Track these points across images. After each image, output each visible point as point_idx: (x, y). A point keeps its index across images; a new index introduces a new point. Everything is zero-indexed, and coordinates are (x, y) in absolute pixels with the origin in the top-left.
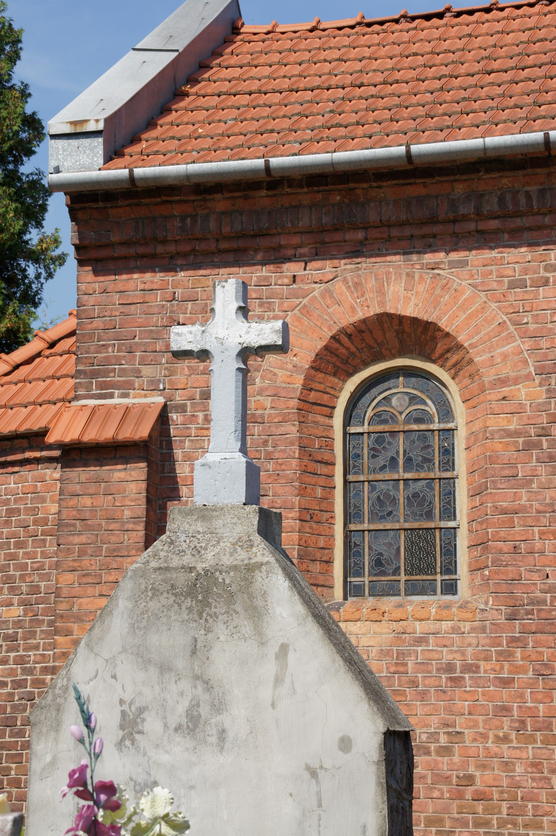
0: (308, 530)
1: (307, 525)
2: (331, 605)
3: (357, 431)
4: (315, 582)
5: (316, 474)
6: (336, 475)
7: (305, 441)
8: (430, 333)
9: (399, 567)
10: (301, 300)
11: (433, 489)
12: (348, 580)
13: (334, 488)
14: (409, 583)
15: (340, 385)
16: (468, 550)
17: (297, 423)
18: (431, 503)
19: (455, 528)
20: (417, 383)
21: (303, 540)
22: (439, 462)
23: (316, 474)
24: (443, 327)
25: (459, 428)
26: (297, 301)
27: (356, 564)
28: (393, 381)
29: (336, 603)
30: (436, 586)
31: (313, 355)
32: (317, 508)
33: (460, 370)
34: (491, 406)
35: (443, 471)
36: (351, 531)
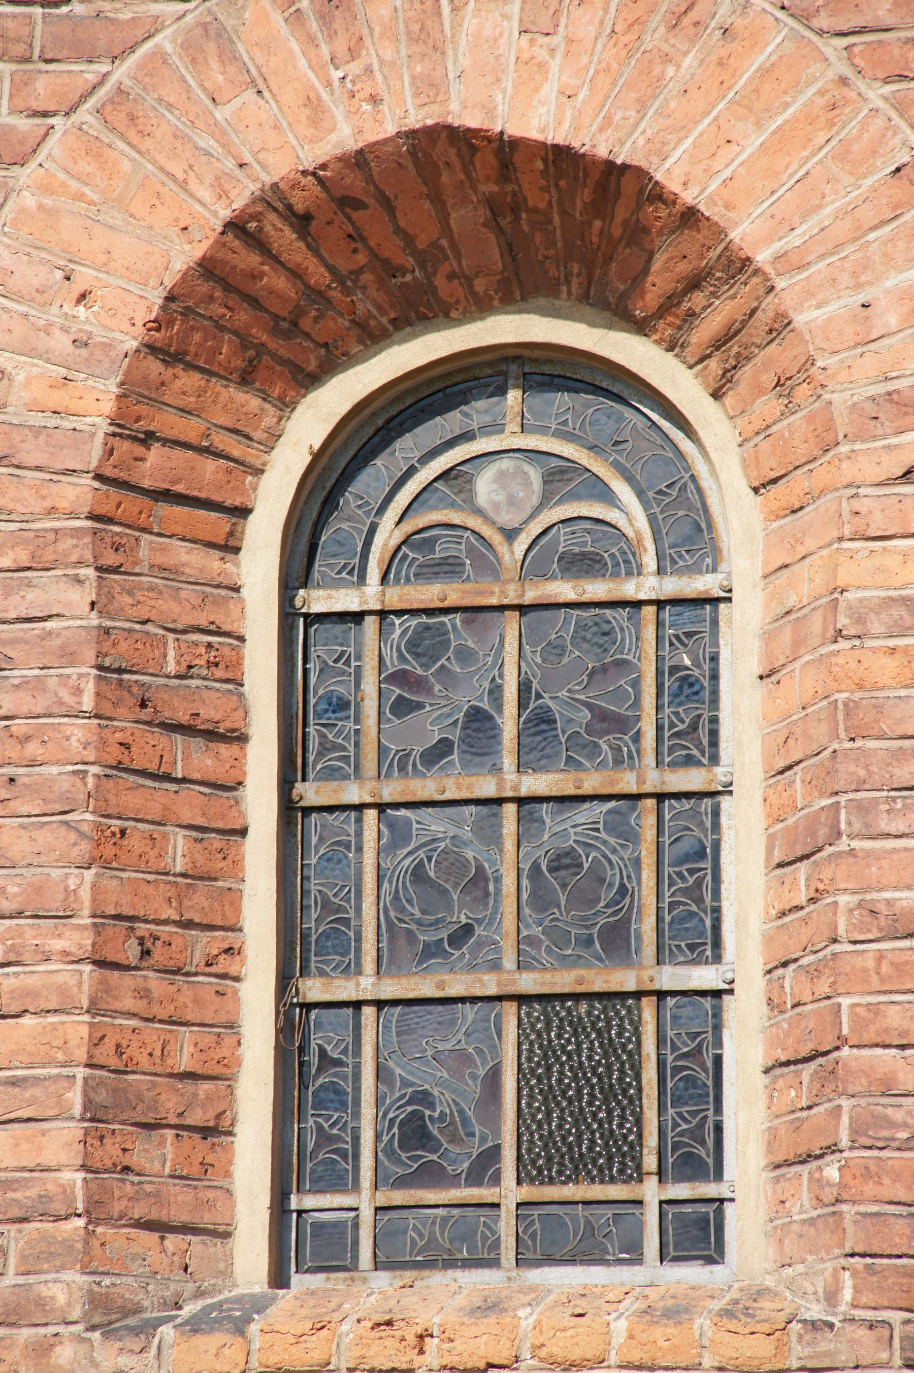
0: (129, 1003)
1: (126, 981)
2: (219, 1306)
3: (338, 607)
4: (154, 1215)
5: (168, 778)
6: (249, 782)
7: (123, 646)
8: (621, 213)
9: (498, 1147)
10: (104, 68)
11: (631, 837)
12: (294, 1202)
13: (243, 832)
14: (536, 1212)
15: (269, 420)
16: (762, 1080)
17: (90, 573)
18: (623, 891)
19: (717, 994)
20: (576, 416)
21: (109, 1045)
22: (659, 729)
23: (168, 778)
24: (673, 185)
25: (735, 595)
26: (91, 72)
27: (324, 1138)
28: (480, 404)
29: (238, 1300)
30: (640, 1226)
31: (156, 298)
32: (170, 913)
33: (742, 360)
34: (856, 505)
35: (673, 765)
36: (308, 1007)
